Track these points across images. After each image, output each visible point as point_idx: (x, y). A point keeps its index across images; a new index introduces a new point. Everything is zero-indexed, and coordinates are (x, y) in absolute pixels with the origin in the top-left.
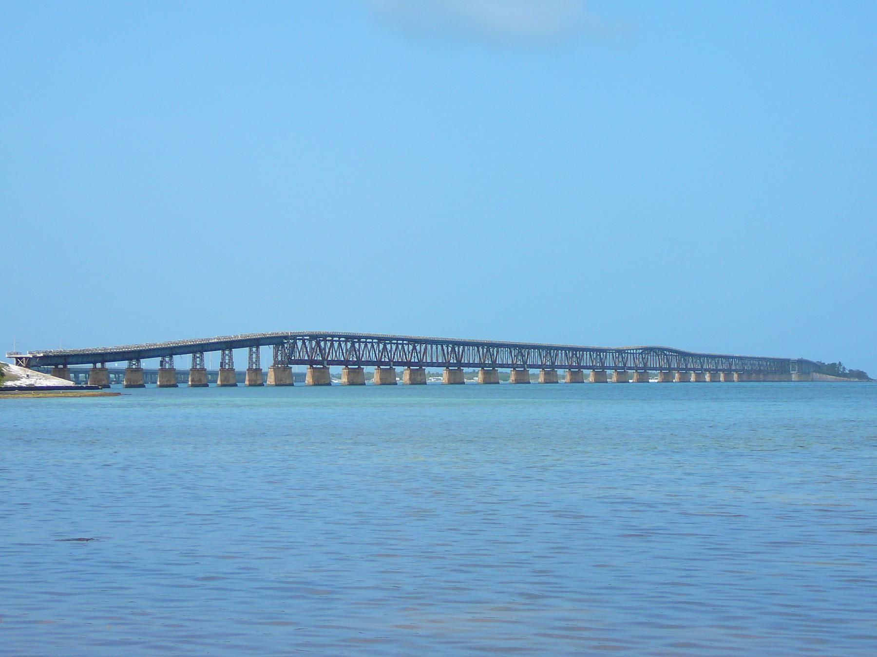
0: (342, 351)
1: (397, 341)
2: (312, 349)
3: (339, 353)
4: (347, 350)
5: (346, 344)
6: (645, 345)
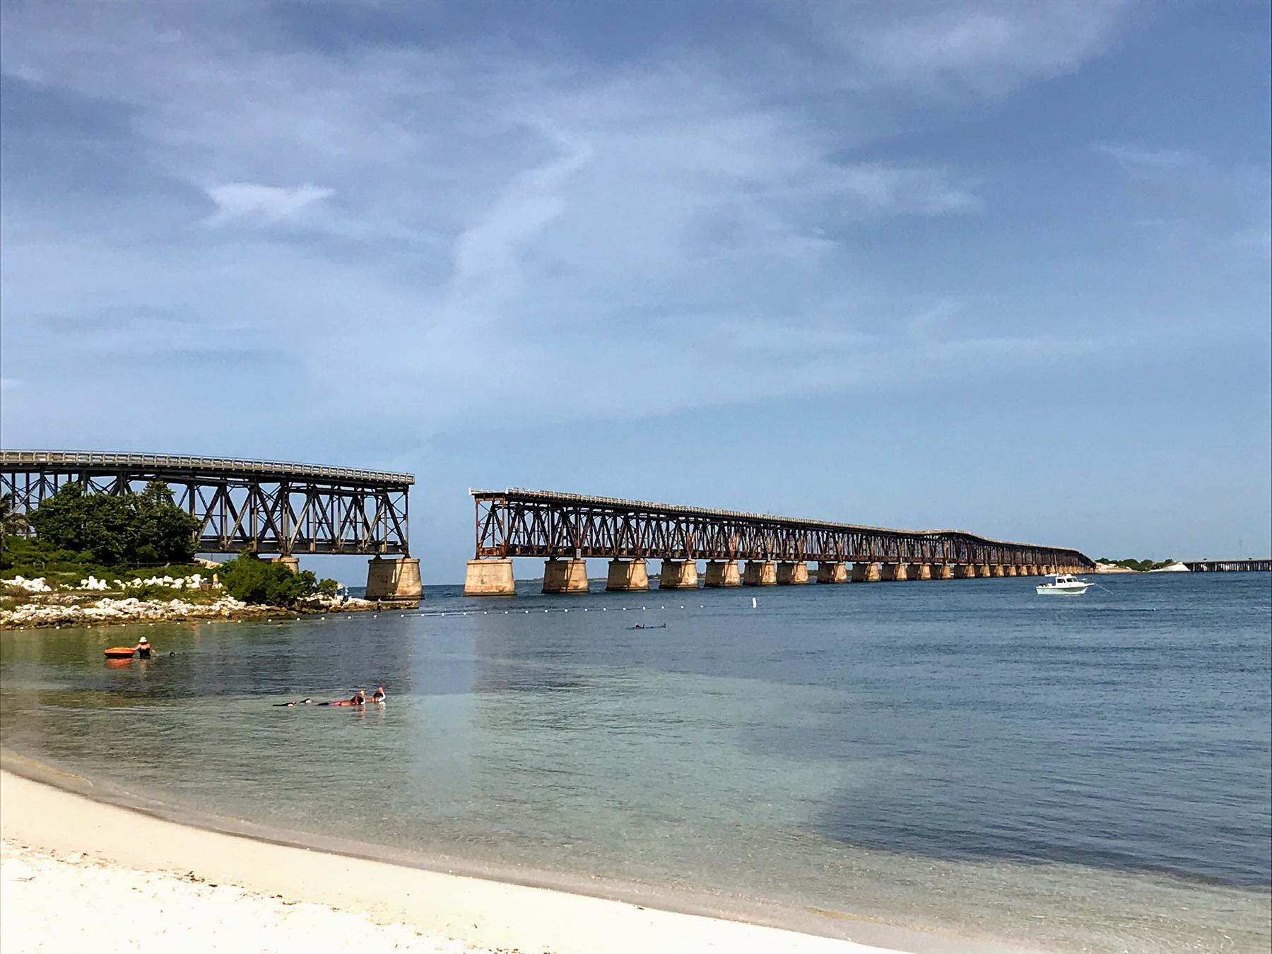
0: (608, 531)
2: (554, 528)
3: (603, 534)
4: (617, 531)
6: (945, 530)
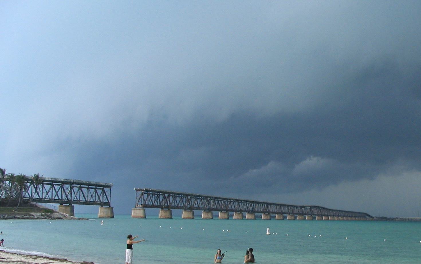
1: (246, 202)
5: (249, 204)
